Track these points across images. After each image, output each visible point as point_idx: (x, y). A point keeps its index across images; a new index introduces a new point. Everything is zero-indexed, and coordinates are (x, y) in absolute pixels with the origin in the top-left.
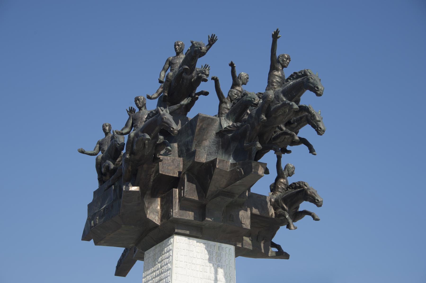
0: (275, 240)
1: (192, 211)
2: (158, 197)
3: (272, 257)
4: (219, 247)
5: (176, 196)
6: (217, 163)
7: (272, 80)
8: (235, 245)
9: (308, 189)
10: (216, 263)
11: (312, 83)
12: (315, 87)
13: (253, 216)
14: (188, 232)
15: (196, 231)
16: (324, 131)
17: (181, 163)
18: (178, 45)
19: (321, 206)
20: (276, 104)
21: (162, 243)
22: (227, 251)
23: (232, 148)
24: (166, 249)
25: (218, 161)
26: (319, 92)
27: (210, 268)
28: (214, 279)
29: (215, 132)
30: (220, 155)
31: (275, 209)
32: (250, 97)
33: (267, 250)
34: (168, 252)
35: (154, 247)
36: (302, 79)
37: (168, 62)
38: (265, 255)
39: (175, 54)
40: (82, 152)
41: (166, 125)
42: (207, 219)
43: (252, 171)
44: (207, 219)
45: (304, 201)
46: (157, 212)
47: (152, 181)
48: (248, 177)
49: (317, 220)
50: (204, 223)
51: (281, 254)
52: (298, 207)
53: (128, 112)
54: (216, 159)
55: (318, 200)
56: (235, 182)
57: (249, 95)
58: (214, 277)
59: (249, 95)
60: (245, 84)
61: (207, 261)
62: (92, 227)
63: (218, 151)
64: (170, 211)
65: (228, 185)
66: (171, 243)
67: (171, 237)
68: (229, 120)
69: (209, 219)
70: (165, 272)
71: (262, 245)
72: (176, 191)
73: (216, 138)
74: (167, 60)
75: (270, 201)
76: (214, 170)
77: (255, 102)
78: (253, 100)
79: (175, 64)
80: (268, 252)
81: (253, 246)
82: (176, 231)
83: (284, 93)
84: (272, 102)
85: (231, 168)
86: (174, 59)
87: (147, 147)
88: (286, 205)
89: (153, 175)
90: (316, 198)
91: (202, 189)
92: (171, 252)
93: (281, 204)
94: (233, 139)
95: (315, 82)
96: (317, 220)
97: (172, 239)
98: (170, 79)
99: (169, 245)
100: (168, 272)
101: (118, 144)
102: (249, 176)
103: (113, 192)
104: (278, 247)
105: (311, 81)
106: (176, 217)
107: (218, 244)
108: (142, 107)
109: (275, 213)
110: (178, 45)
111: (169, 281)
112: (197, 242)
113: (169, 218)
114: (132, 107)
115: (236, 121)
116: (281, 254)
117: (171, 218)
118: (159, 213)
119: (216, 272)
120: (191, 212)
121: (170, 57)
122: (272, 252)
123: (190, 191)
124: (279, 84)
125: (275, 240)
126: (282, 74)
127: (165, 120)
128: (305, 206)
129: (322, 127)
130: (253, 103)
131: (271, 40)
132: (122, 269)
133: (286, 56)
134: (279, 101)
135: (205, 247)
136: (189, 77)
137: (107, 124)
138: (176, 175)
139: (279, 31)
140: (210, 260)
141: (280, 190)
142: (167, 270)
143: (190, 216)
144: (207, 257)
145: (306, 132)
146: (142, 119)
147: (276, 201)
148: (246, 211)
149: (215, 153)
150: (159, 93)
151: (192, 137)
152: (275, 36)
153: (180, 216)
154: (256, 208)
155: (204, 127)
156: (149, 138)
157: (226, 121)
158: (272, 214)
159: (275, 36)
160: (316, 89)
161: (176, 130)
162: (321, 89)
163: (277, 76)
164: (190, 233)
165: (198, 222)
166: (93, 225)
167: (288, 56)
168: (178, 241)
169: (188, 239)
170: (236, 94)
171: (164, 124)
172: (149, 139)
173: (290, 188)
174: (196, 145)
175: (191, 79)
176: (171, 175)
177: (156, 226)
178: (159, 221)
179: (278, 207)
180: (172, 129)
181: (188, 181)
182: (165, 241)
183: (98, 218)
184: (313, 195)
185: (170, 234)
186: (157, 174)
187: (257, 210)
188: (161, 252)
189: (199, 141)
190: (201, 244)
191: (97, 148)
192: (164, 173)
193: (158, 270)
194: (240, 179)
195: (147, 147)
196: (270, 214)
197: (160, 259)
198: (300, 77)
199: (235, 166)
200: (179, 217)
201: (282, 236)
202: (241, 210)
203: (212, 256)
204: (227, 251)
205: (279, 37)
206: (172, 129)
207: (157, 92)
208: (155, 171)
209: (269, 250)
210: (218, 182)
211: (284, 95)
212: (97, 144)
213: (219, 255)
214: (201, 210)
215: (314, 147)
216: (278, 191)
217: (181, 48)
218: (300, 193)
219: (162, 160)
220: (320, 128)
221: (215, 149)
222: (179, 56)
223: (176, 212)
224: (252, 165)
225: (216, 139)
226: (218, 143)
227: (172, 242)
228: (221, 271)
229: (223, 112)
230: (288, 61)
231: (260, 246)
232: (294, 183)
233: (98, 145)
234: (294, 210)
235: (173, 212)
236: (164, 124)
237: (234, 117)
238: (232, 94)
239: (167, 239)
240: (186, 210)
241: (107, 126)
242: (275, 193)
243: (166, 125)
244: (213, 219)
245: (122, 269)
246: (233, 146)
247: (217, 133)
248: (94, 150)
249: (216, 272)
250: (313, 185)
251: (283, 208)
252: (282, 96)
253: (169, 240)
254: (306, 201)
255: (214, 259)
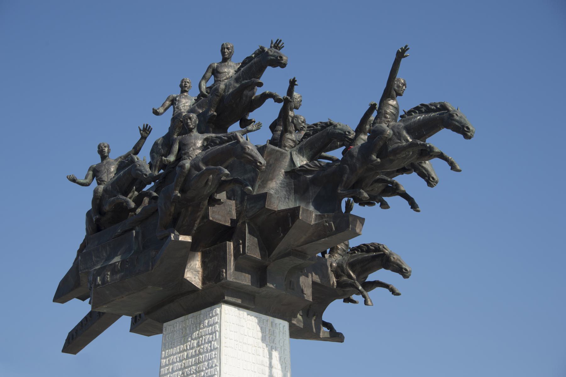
0: (326, 317)
1: (249, 274)
2: (198, 251)
3: (325, 339)
4: (272, 322)
5: (230, 252)
6: (300, 212)
7: (385, 111)
8: (289, 321)
9: (391, 254)
10: (269, 343)
11: (457, 121)
12: (463, 126)
13: (314, 283)
14: (239, 301)
15: (248, 301)
16: (437, 182)
17: (234, 208)
18: (228, 48)
19: (408, 277)
20: (396, 143)
21: (198, 313)
22: (281, 329)
23: (311, 194)
24: (206, 321)
25: (301, 209)
26: (469, 134)
27: (263, 349)
28: (268, 365)
29: (283, 171)
30: (292, 201)
31: (337, 276)
32: (341, 129)
33: (319, 330)
34: (209, 325)
35: (183, 317)
36: (440, 114)
37: (211, 70)
38: (316, 336)
39: (220, 59)
40: (74, 180)
41: (249, 157)
42: (269, 285)
43: (349, 227)
44: (269, 285)
45: (383, 269)
46: (198, 271)
47: (195, 228)
48: (340, 235)
49: (398, 294)
50: (263, 290)
51: (336, 336)
52: (366, 277)
53: (140, 130)
54: (299, 207)
55: (406, 270)
56: (318, 240)
57: (339, 127)
58: (268, 363)
59: (339, 127)
60: (297, 109)
61: (260, 341)
62: (99, 285)
63: (289, 196)
64: (223, 272)
65: (306, 242)
66: (217, 315)
67: (218, 305)
68: (303, 156)
69: (271, 286)
70: (207, 352)
71: (313, 322)
72: (231, 246)
73: (285, 178)
74: (210, 66)
75: (331, 265)
76: (293, 222)
77: (350, 137)
78: (347, 133)
79: (222, 73)
80: (320, 332)
81: (304, 323)
82: (226, 298)
83: (409, 130)
84: (390, 139)
85: (316, 220)
86: (221, 66)
87: (210, 184)
88: (354, 272)
89: (198, 221)
90: (404, 267)
91: (267, 246)
92: (217, 326)
93: (347, 270)
94: (313, 181)
95: (462, 120)
96: (398, 294)
97: (218, 309)
98: (221, 94)
99: (213, 316)
100: (214, 353)
101: (146, 175)
102: (342, 233)
103: (134, 239)
104: (328, 325)
105: (456, 117)
106: (231, 280)
107: (271, 319)
108: (193, 129)
109: (337, 282)
110: (228, 48)
111: (216, 365)
112: (248, 315)
113: (220, 280)
114: (147, 125)
115: (311, 159)
116: (336, 336)
117: (223, 281)
118: (200, 273)
119: (271, 357)
120: (247, 275)
121: (214, 63)
122: (324, 332)
123: (252, 247)
124: (394, 117)
125: (326, 317)
126: (397, 104)
127: (247, 150)
128: (380, 275)
129: (435, 177)
130: (348, 138)
131: (394, 57)
132: (76, 341)
133: (403, 81)
134: (400, 140)
135: (257, 321)
136: (250, 93)
137: (106, 145)
138: (228, 224)
139: (408, 49)
140: (263, 339)
141: (339, 252)
142: (211, 350)
143: (245, 280)
144: (260, 335)
145: (408, 182)
146: (195, 145)
147: (340, 266)
148: (307, 276)
149: (285, 198)
150: (166, 107)
151: (253, 174)
152: (400, 55)
153: (235, 279)
154: (316, 274)
155: (271, 162)
156: (228, 172)
157: (298, 156)
158: (334, 282)
159: (400, 55)
160: (466, 129)
161: (264, 165)
162: (472, 131)
163: (392, 105)
164: (242, 302)
165: (255, 289)
166: (100, 283)
167: (404, 81)
168: (227, 312)
169: (239, 310)
170: (303, 122)
171: (246, 155)
172: (228, 174)
173: (358, 251)
174: (259, 185)
175: (252, 96)
176: (223, 223)
177: (195, 289)
178: (200, 284)
179: (342, 274)
180: (258, 164)
181: (249, 233)
182: (203, 311)
183: (109, 273)
184: (398, 262)
185: (218, 300)
186: (205, 220)
187: (317, 276)
188: (198, 325)
189: (263, 181)
190: (253, 317)
191: (90, 176)
192: (214, 220)
193: (192, 348)
194: (328, 237)
195: (210, 184)
196: (332, 282)
197: (195, 334)
198: (434, 111)
199: (322, 218)
200: (235, 281)
201: (335, 312)
202: (301, 275)
203: (264, 334)
204: (281, 329)
205: (406, 56)
206: (258, 164)
207: (163, 105)
208: (201, 217)
209: (320, 329)
210: (292, 239)
211: (408, 133)
212: (89, 170)
213: (272, 334)
214: (261, 274)
215: (417, 201)
216: (337, 253)
217: (231, 53)
218: (377, 257)
219: (223, 203)
220: (433, 178)
221: (284, 192)
222: (226, 63)
223: (231, 273)
224: (349, 220)
225: (286, 180)
226: (288, 185)
227: (218, 312)
228: (275, 354)
229: (287, 145)
230: (404, 87)
231: (311, 323)
232: (364, 245)
233: (91, 173)
234: (363, 280)
235: (226, 273)
236: (246, 155)
237: (311, 152)
238: (298, 121)
239: (209, 309)
240: (242, 272)
241: (105, 147)
242: (333, 256)
243: (249, 157)
244: (275, 285)
245: (76, 341)
246: (313, 192)
247: (286, 173)
248: (86, 178)
249: (271, 357)
250: (394, 248)
251: (350, 276)
252: (405, 133)
253: (212, 310)
254: (386, 268)
255: (267, 337)
